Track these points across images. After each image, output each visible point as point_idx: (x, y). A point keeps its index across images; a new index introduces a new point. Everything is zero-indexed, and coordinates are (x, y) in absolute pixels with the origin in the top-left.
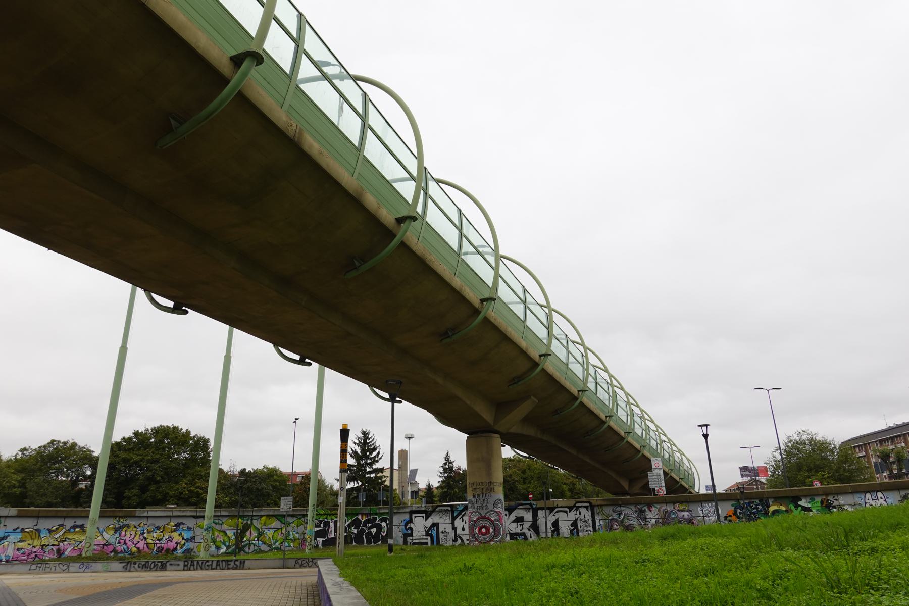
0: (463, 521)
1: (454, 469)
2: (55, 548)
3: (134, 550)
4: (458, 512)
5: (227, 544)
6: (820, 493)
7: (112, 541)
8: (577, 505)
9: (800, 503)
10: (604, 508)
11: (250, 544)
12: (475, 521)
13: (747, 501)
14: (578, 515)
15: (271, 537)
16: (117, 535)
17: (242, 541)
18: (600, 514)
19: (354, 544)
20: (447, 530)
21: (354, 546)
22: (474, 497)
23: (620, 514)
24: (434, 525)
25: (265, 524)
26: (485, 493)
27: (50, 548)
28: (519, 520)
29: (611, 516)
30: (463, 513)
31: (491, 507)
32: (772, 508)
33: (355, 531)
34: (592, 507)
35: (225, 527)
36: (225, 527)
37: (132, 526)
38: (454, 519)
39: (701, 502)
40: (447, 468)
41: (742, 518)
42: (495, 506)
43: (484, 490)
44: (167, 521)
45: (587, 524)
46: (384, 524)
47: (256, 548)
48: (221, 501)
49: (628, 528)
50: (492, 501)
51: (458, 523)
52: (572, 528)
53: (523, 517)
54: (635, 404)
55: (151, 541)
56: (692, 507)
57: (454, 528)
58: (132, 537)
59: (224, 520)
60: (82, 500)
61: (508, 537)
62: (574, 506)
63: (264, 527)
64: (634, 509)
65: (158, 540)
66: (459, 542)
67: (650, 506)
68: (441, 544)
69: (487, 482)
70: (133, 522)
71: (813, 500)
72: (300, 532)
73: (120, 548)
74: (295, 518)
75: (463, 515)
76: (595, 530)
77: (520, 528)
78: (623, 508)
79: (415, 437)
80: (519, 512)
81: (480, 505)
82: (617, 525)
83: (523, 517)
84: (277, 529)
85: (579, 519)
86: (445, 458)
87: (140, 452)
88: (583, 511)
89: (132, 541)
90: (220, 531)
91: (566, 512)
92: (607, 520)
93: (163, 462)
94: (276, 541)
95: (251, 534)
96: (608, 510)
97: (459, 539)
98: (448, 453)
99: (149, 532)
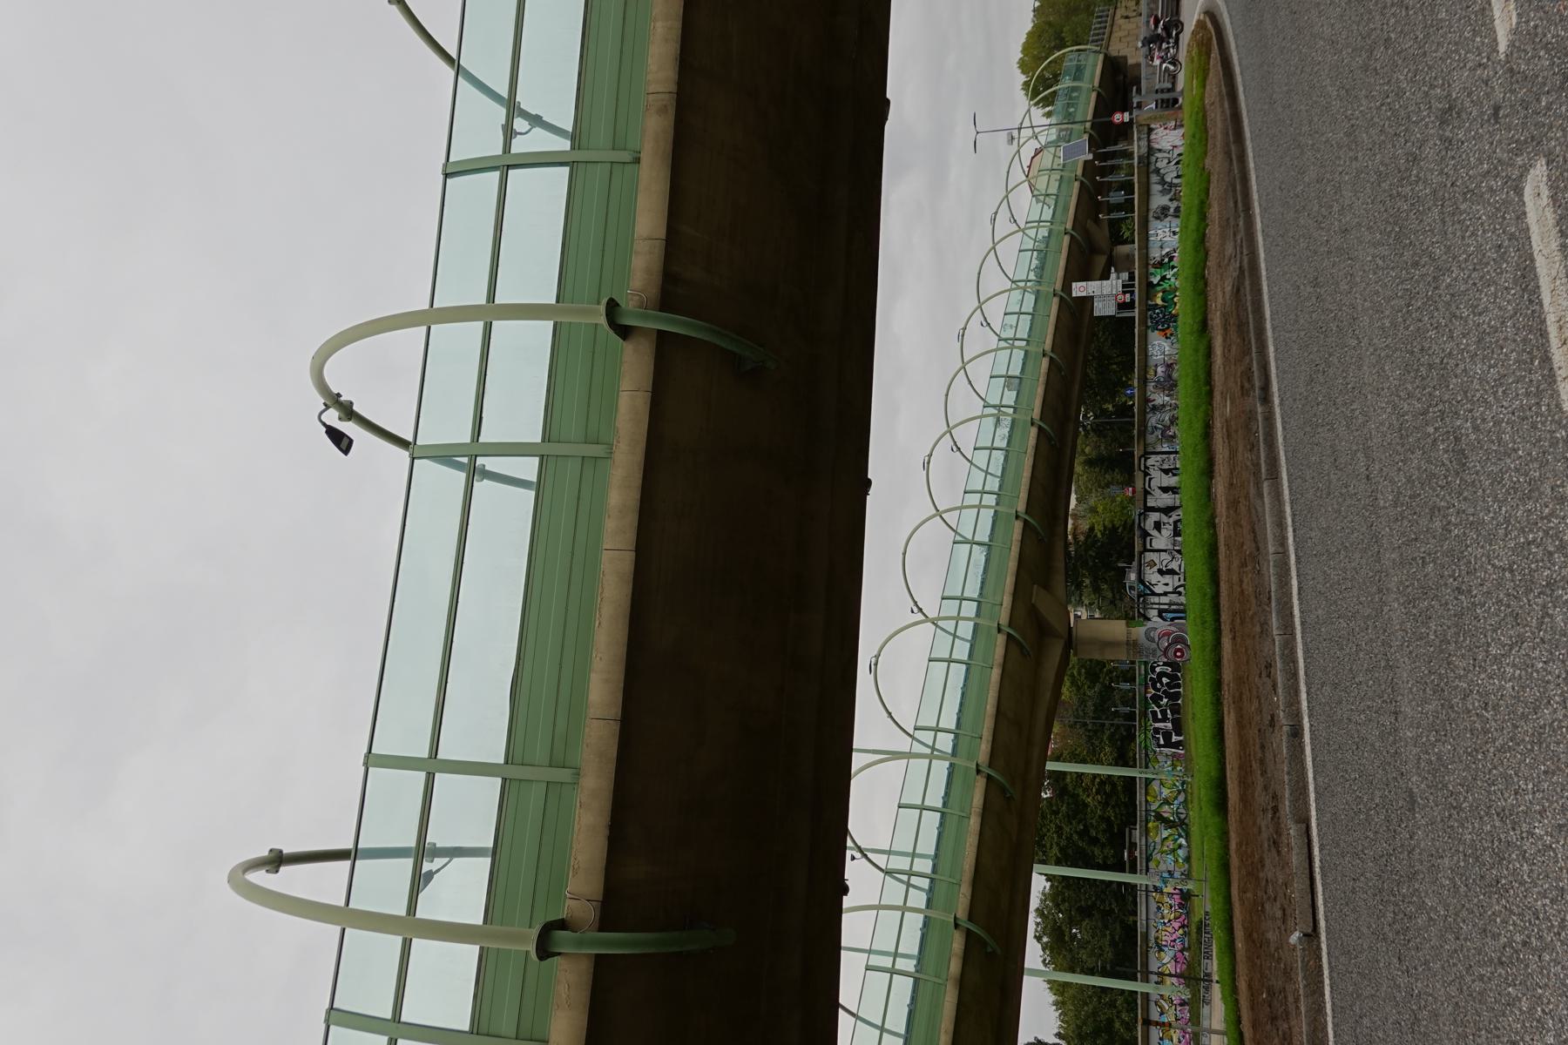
2: (1179, 1008)
3: (1181, 931)
5: (1177, 837)
6: (1145, 270)
7: (1171, 954)
8: (1143, 469)
9: (1155, 282)
11: (1177, 813)
13: (1149, 320)
15: (1169, 791)
16: (1166, 949)
17: (1174, 822)
19: (1179, 702)
21: (1184, 691)
25: (1156, 797)
27: (1178, 1013)
28: (1158, 526)
31: (1154, 646)
32: (1159, 302)
33: (1165, 700)
34: (1146, 455)
35: (1158, 839)
36: (1158, 839)
37: (1156, 934)
38: (1154, 594)
39: (1146, 355)
41: (1168, 325)
42: (1153, 640)
44: (1151, 899)
46: (1158, 670)
47: (1181, 807)
48: (1110, 758)
49: (1173, 420)
50: (1147, 643)
51: (1158, 590)
53: (1155, 522)
54: (1028, 115)
55: (1173, 915)
56: (1151, 363)
57: (1165, 594)
58: (1168, 934)
59: (1150, 840)
60: (1108, 908)
61: (1179, 539)
63: (1159, 798)
64: (1151, 415)
65: (1171, 908)
66: (1181, 589)
67: (1148, 401)
70: (1153, 934)
71: (1152, 274)
72: (1164, 759)
73: (1178, 946)
74: (1150, 764)
75: (1150, 584)
76: (1176, 452)
77: (1167, 526)
78: (1149, 424)
80: (1149, 525)
83: (1155, 522)
84: (1161, 784)
87: (1048, 845)
88: (1150, 462)
89: (1172, 934)
90: (1162, 845)
91: (1150, 479)
93: (1060, 821)
94: (1175, 785)
95: (1166, 811)
96: (1151, 438)
99: (1163, 918)
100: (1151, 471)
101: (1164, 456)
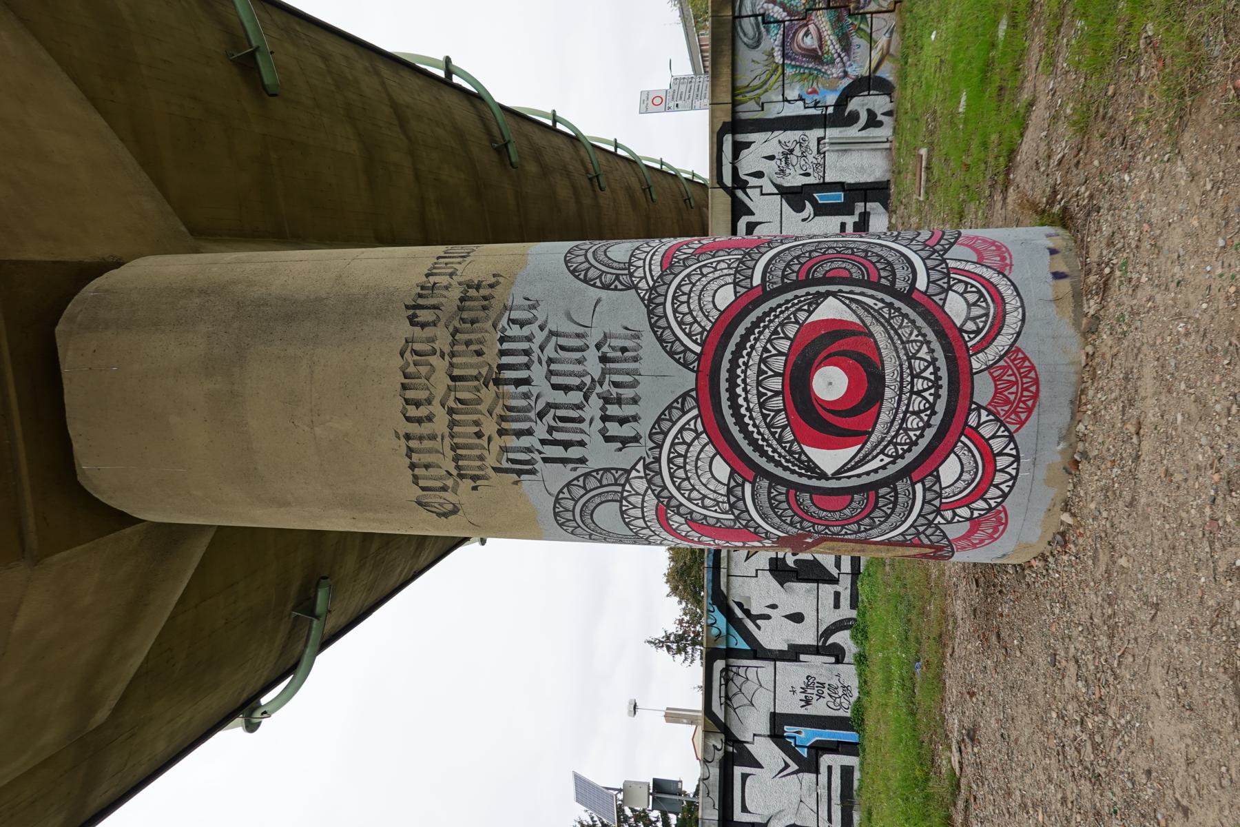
0: (768, 617)
1: (681, 633)
4: (733, 631)
8: (728, 180)
10: (744, 79)
12: (743, 467)
14: (764, 182)
18: (763, 99)
20: (800, 682)
22: (522, 469)
23: (766, 20)
24: (776, 736)
26: (492, 357)
29: (771, 55)
30: (739, 613)
38: (757, 652)
40: (678, 646)
43: (467, 364)
45: (797, 152)
51: (773, 636)
52: (809, 208)
57: (793, 653)
62: (731, 192)
68: (848, 714)
69: (406, 330)
75: (747, 612)
79: (633, 698)
81: (595, 403)
82: (806, 34)
85: (779, 181)
86: (657, 647)
92: (789, 71)
97: (830, 641)
98: (650, 642)
100: (754, 199)
101: (791, 136)
